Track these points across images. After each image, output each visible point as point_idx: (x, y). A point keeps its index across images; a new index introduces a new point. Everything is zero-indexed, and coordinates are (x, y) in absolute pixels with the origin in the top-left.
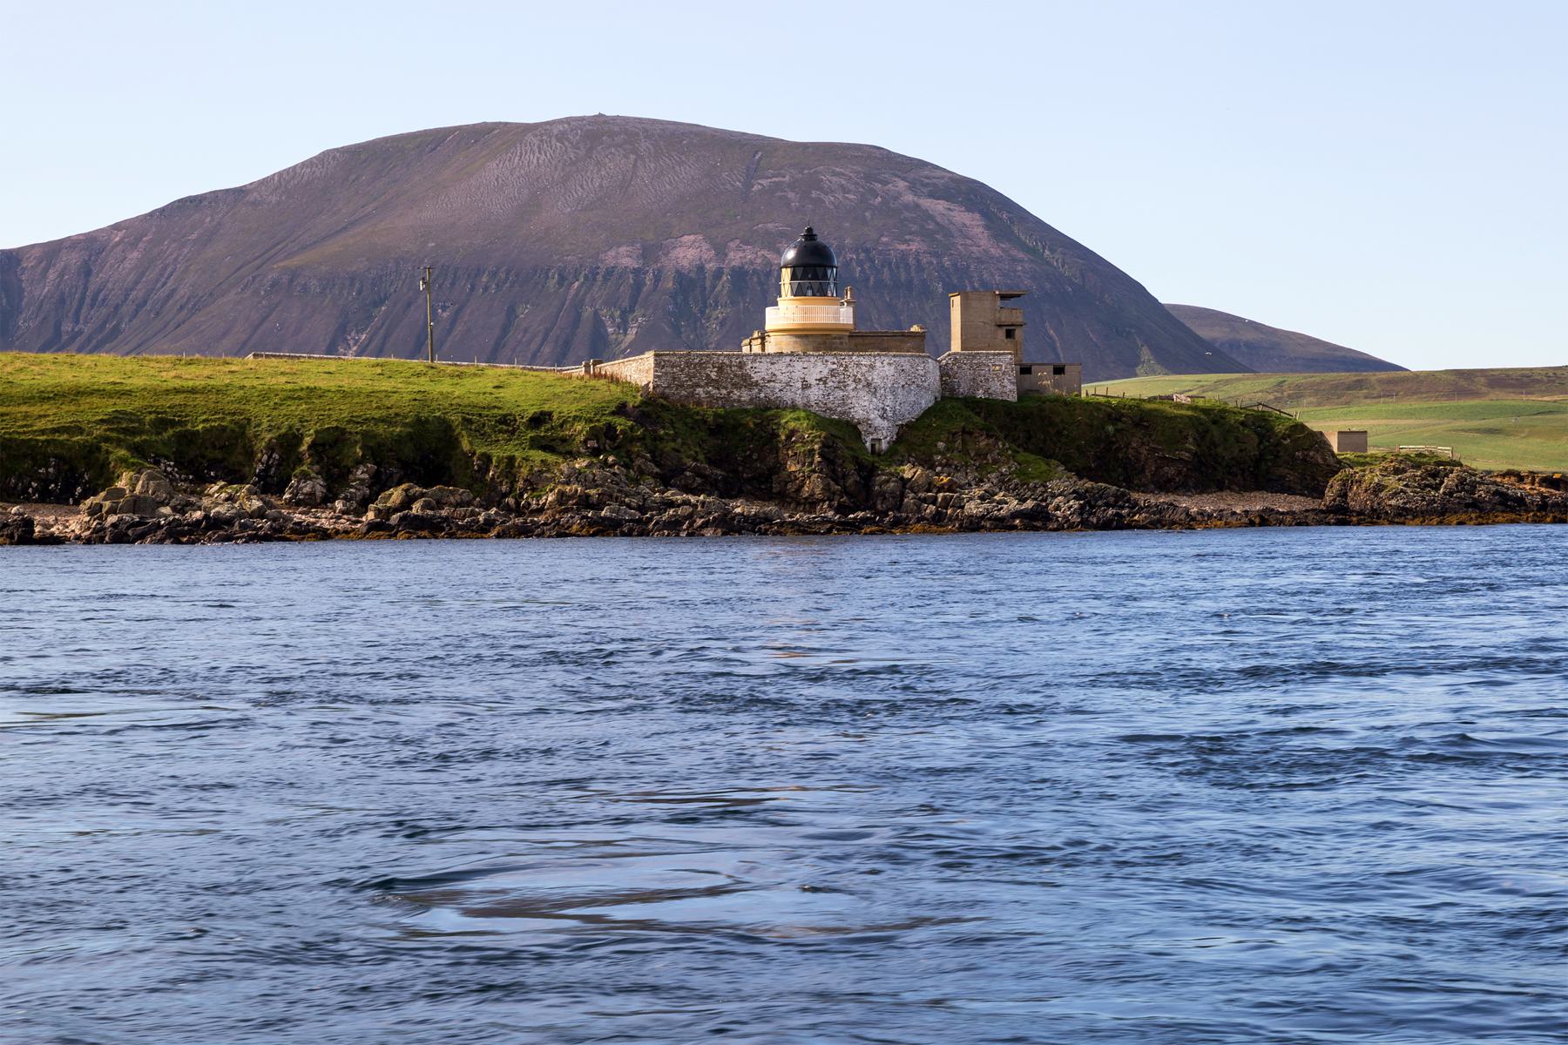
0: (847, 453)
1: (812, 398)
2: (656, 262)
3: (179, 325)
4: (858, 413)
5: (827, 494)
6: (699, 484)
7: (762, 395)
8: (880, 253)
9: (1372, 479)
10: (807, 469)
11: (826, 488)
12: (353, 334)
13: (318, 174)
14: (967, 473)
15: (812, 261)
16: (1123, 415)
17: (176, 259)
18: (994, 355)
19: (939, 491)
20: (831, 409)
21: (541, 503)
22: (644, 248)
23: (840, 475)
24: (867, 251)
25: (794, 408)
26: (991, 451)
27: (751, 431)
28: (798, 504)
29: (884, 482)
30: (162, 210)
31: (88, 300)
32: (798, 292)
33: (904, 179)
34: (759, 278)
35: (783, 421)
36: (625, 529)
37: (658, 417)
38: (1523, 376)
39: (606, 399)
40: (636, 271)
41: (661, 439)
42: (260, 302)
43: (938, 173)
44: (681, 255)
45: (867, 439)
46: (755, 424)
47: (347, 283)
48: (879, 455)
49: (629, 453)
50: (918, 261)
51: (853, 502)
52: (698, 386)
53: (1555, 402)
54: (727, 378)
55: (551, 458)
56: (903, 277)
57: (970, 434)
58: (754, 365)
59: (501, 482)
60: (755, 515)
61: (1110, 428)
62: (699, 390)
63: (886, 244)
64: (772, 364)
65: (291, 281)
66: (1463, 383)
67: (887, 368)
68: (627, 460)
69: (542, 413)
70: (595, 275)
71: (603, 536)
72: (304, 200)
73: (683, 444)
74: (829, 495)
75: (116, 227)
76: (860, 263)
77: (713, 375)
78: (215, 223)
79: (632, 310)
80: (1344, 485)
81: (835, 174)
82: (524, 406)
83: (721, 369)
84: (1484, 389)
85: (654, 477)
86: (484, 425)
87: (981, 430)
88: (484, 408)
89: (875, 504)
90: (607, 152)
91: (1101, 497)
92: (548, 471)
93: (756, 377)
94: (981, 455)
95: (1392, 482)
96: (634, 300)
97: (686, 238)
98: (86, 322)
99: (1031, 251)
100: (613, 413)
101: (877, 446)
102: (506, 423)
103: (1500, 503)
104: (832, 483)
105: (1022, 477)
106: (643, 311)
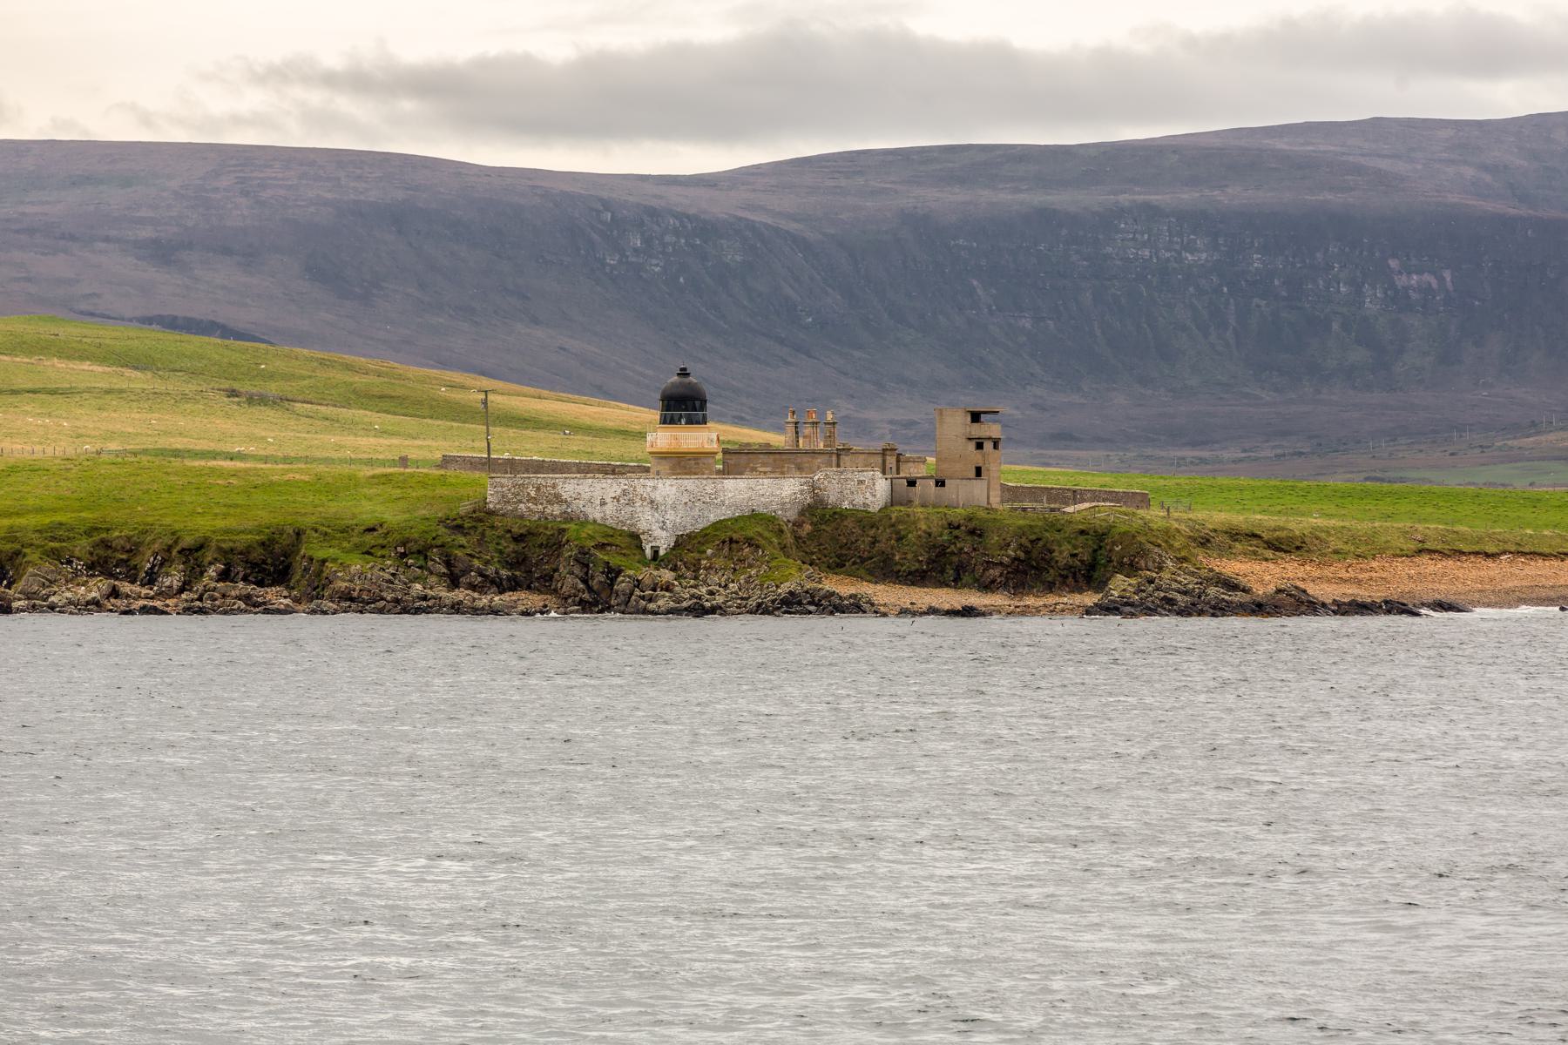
4: (642, 526)
20: (622, 522)
62: (522, 506)
77: (533, 494)
83: (538, 489)
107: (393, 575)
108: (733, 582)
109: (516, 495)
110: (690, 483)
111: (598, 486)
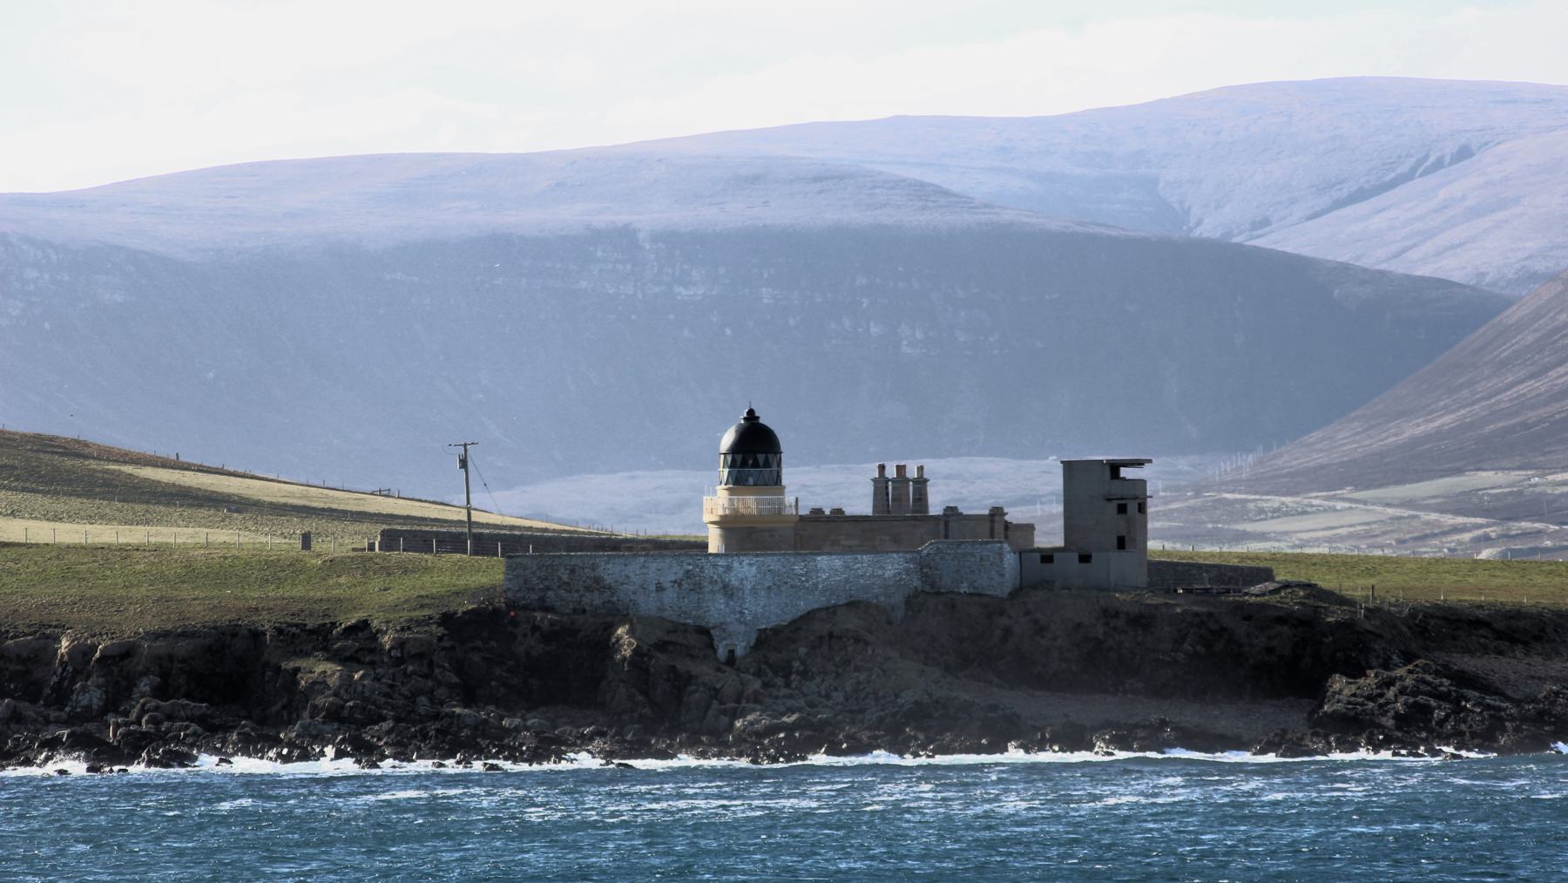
1: (666, 601)
20: (685, 613)
77: (565, 578)
83: (573, 571)
93: (608, 580)
107: (391, 686)
108: (836, 689)
110: (773, 562)
111: (653, 566)
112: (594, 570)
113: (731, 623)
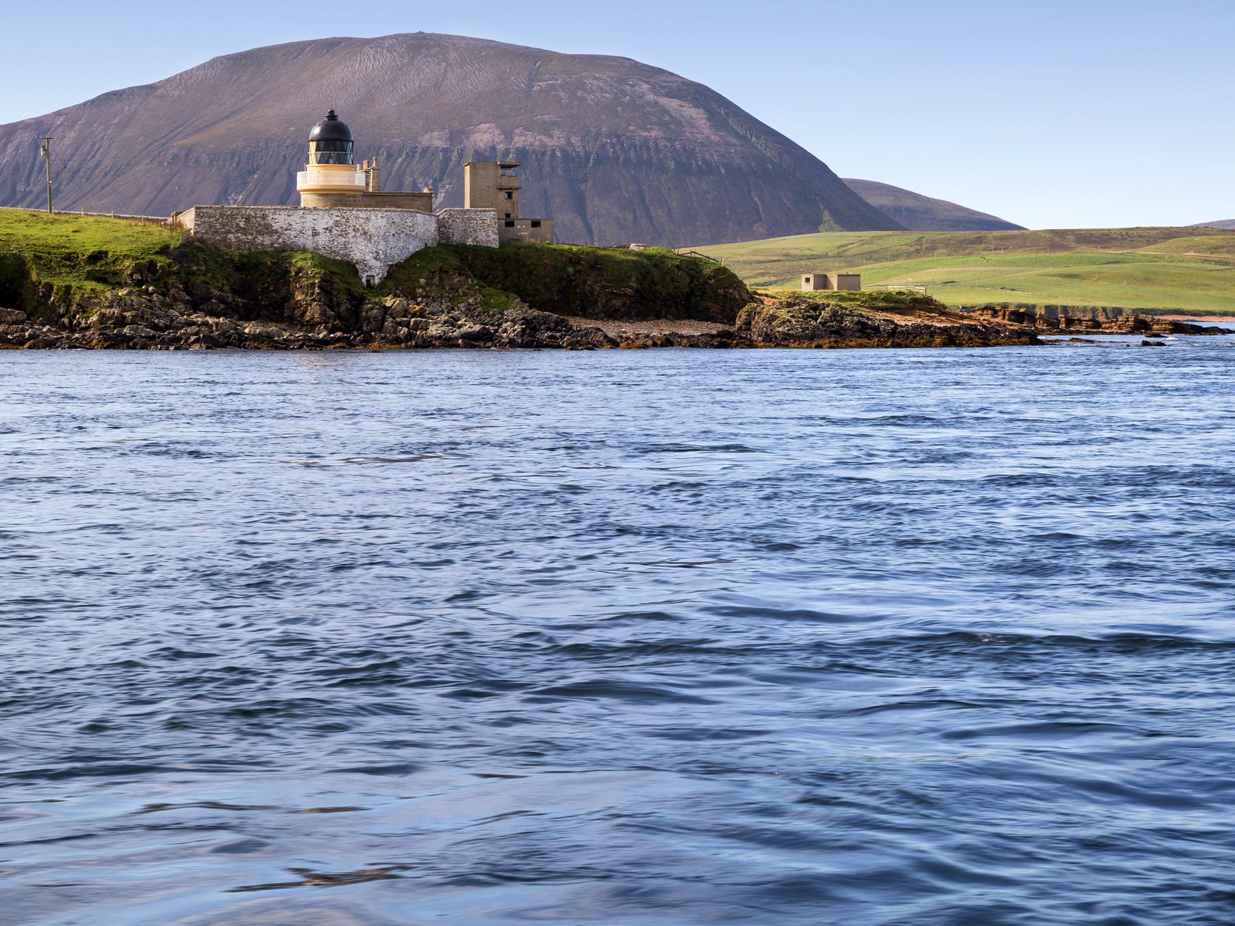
0: (343, 286)
2: (460, 144)
3: (104, 188)
4: (356, 255)
5: (324, 318)
6: (222, 310)
7: (281, 240)
8: (628, 138)
9: (769, 311)
10: (309, 298)
11: (323, 314)
12: (232, 196)
13: (209, 75)
14: (441, 303)
15: (333, 136)
16: (581, 259)
17: (102, 138)
18: (481, 211)
19: (413, 317)
20: (335, 252)
21: (89, 322)
22: (451, 133)
23: (335, 303)
24: (618, 136)
25: (304, 250)
26: (461, 286)
27: (269, 268)
28: (303, 325)
29: (370, 309)
30: (93, 101)
31: (36, 168)
32: (323, 160)
33: (647, 83)
34: (536, 156)
35: (294, 261)
36: (131, 344)
37: (194, 256)
38: (1102, 235)
39: (154, 242)
40: (445, 150)
41: (194, 273)
42: (164, 171)
43: (673, 79)
44: (479, 139)
45: (363, 276)
46: (272, 263)
47: (229, 157)
48: (373, 288)
49: (166, 284)
50: (657, 144)
51: (344, 325)
52: (230, 232)
53: (1122, 254)
54: (253, 227)
55: (99, 287)
56: (645, 156)
57: (446, 272)
58: (275, 217)
59: (60, 305)
60: (259, 333)
61: (571, 270)
62: (231, 236)
63: (632, 131)
64: (289, 216)
65: (187, 155)
66: (1057, 239)
67: (380, 220)
68: (164, 290)
69: (100, 252)
70: (413, 151)
71: (114, 348)
72: (199, 95)
73: (213, 277)
74: (325, 319)
75: (59, 113)
76: (613, 146)
77: (242, 224)
78: (132, 111)
79: (441, 180)
80: (749, 315)
81: (595, 78)
82: (88, 246)
83: (248, 219)
84: (1073, 244)
85: (185, 303)
86: (51, 261)
87: (455, 269)
88: (54, 247)
89: (362, 326)
90: (425, 61)
91: (545, 323)
92: (96, 297)
93: (276, 226)
94: (454, 289)
95: (784, 314)
96: (443, 172)
97: (482, 126)
98: (35, 185)
99: (743, 138)
100: (157, 253)
101: (372, 281)
102: (70, 260)
103: (859, 331)
104: (328, 309)
105: (484, 307)
106: (449, 180)
109: (224, 225)
110: (396, 215)
112: (264, 219)
113: (370, 260)
